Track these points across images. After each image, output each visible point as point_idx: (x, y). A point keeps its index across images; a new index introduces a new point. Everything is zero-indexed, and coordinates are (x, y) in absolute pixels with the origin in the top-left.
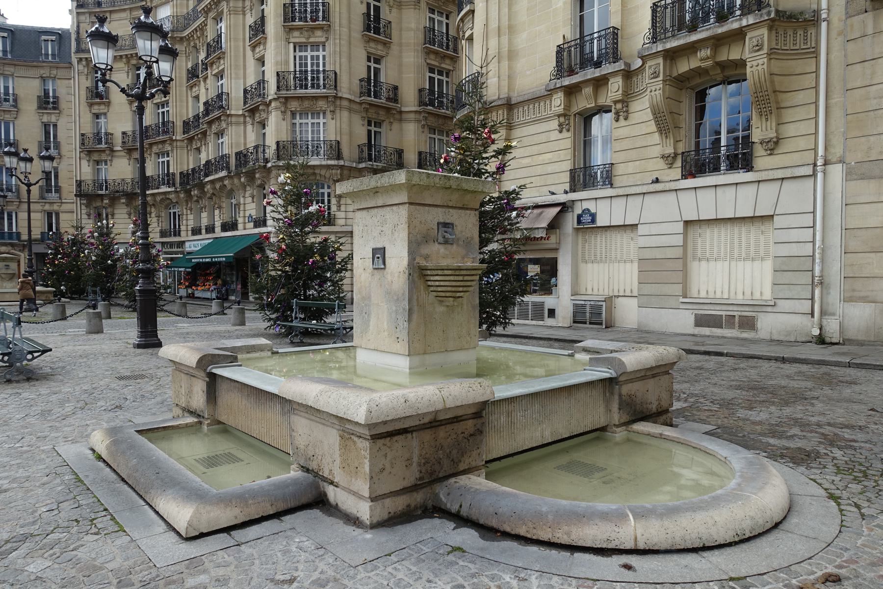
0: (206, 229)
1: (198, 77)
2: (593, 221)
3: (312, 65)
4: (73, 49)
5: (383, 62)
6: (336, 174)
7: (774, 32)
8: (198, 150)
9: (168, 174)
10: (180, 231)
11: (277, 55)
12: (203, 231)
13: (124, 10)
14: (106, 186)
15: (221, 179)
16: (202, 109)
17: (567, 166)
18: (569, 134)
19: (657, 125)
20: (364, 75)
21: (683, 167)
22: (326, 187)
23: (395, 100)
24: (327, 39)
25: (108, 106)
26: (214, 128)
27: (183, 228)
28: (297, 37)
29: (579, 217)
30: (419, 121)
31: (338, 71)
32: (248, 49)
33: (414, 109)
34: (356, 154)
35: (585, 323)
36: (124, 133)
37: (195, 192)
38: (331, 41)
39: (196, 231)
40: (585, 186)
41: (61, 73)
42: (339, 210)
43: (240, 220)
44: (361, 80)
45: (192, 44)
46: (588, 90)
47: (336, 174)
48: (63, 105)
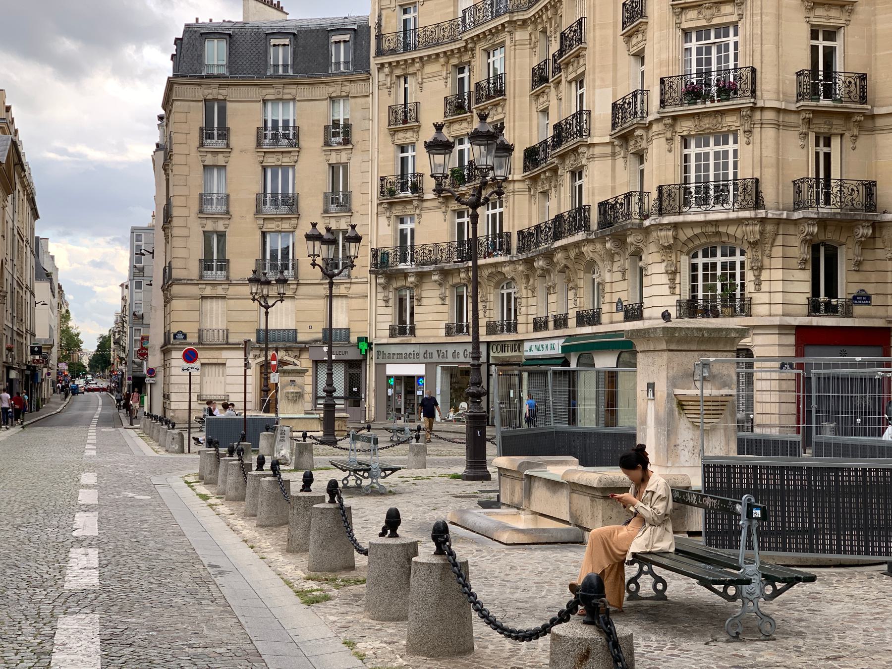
0: (555, 322)
1: (547, 81)
2: (185, 338)
5: (840, 37)
6: (753, 232)
8: (545, 194)
10: (516, 324)
12: (551, 324)
14: (412, 255)
15: (577, 245)
16: (551, 133)
19: (66, 560)
20: (805, 64)
22: (738, 252)
23: (863, 99)
24: (741, 16)
25: (418, 132)
26: (570, 163)
27: (521, 319)
31: (757, 66)
32: (621, 39)
37: (540, 263)
41: (354, 88)
42: (758, 291)
43: (605, 308)
44: (799, 74)
45: (540, 27)
47: (753, 232)
48: (356, 136)
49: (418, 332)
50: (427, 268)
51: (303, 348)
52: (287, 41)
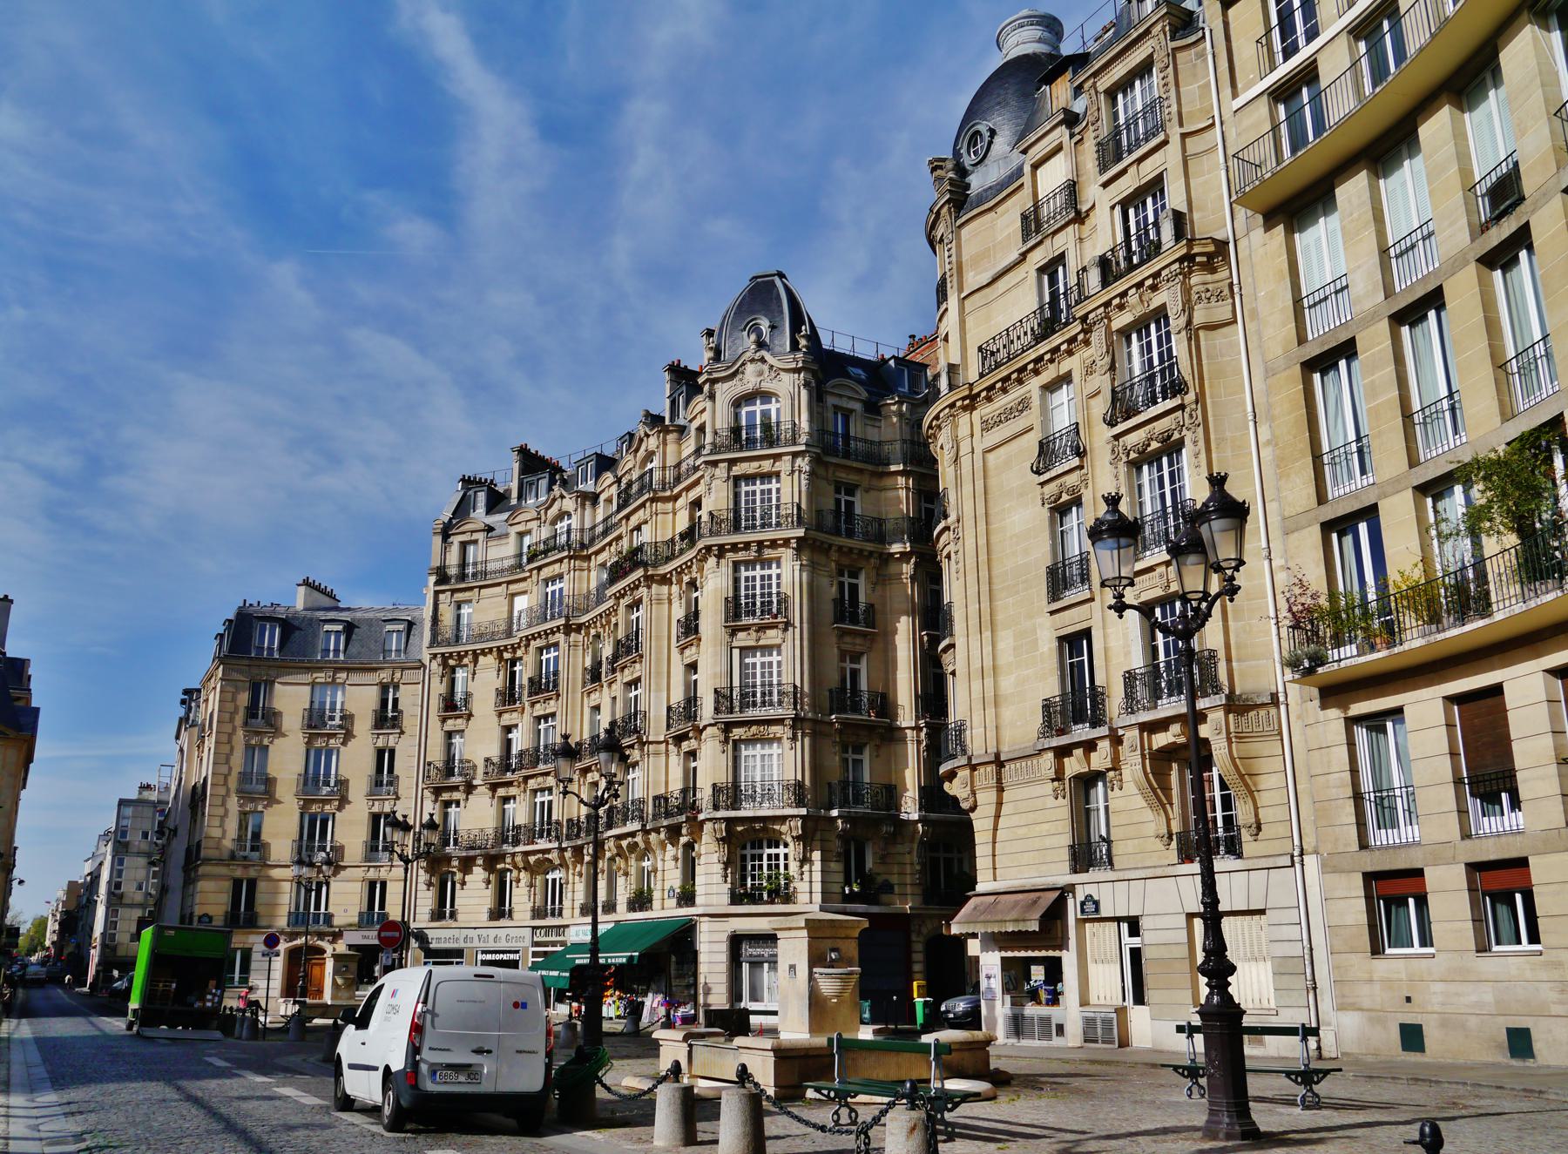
2: (1097, 910)
3: (763, 675)
10: (561, 910)
13: (499, 584)
15: (632, 834)
17: (1066, 840)
21: (1180, 850)
27: (567, 903)
29: (1083, 904)
35: (1096, 1041)
36: (487, 760)
43: (657, 895)
46: (1078, 752)
49: (460, 917)
50: (472, 853)
52: (340, 628)
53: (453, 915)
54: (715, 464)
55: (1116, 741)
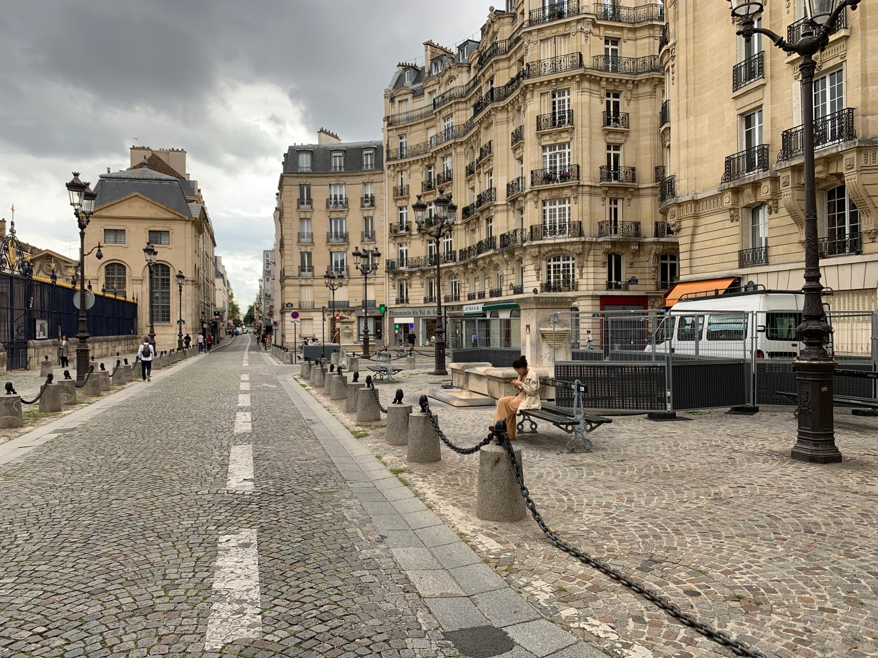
4: (385, 159)
5: (622, 149)
7: (863, 155)
8: (473, 231)
9: (451, 252)
11: (534, 157)
12: (477, 297)
13: (420, 123)
15: (490, 256)
16: (476, 199)
18: (738, 223)
20: (604, 163)
24: (572, 139)
26: (485, 215)
27: (462, 294)
28: (547, 141)
30: (655, 195)
31: (580, 164)
33: (651, 185)
34: (597, 231)
37: (471, 266)
38: (575, 140)
39: (471, 297)
40: (755, 262)
42: (581, 278)
43: (504, 288)
44: (601, 168)
46: (749, 191)
49: (410, 302)
50: (414, 269)
51: (352, 310)
53: (407, 300)
54: (530, 32)
55: (775, 180)
